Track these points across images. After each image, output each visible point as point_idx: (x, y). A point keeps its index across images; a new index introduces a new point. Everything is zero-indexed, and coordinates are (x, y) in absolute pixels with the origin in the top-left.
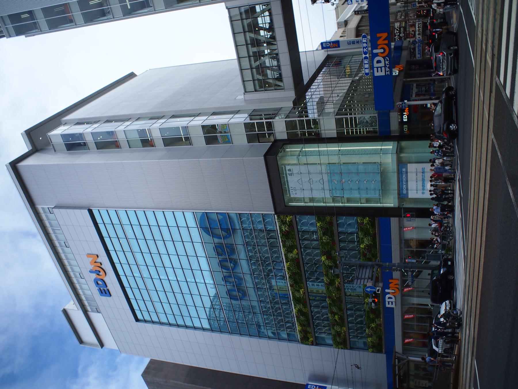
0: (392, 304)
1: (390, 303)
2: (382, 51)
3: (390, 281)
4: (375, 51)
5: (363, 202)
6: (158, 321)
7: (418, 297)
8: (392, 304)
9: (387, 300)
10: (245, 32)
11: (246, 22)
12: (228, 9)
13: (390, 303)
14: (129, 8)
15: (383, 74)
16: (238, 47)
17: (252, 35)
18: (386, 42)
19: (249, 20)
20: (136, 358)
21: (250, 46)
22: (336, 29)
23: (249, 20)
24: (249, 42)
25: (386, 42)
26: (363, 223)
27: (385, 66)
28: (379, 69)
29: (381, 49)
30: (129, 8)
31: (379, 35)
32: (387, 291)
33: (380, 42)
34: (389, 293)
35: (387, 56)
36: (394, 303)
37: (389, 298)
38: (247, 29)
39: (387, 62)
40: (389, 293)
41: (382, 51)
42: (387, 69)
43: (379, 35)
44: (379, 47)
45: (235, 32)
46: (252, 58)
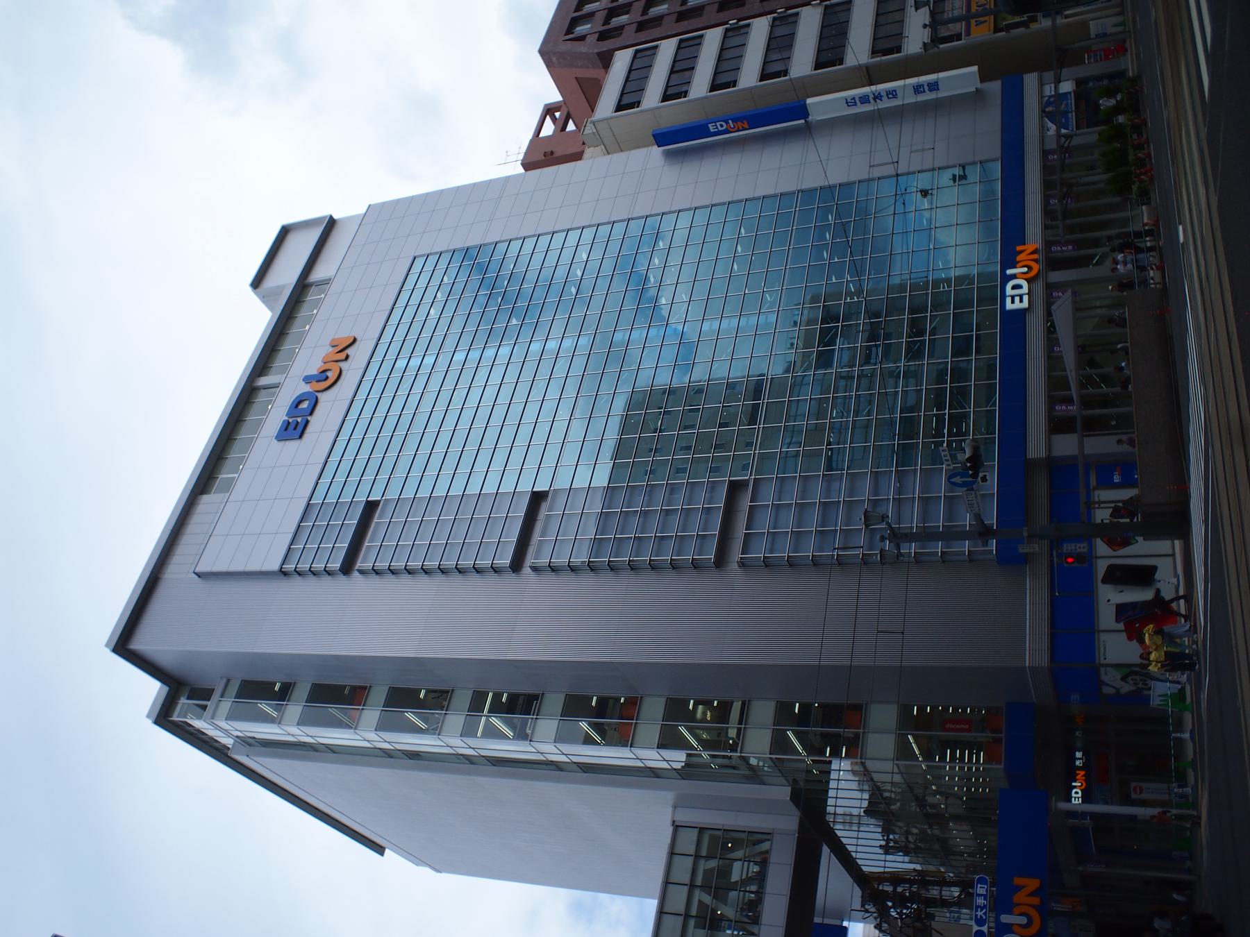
0: (1021, 301)
1: (1017, 299)
2: (1023, 920)
3: (1019, 248)
4: (1005, 919)
6: (548, 118)
8: (1021, 301)
9: (1009, 291)
10: (692, 886)
11: (703, 865)
12: (677, 827)
13: (1017, 299)
14: (504, 700)
16: (665, 916)
17: (707, 899)
19: (713, 864)
21: (692, 922)
23: (713, 864)
24: (694, 912)
29: (1021, 914)
30: (504, 700)
31: (1018, 881)
32: (1009, 272)
33: (1020, 897)
34: (1014, 277)
36: (1026, 298)
37: (1014, 287)
38: (699, 882)
40: (1014, 277)
41: (1023, 920)
43: (1018, 881)
45: (677, 851)
46: (692, 922)
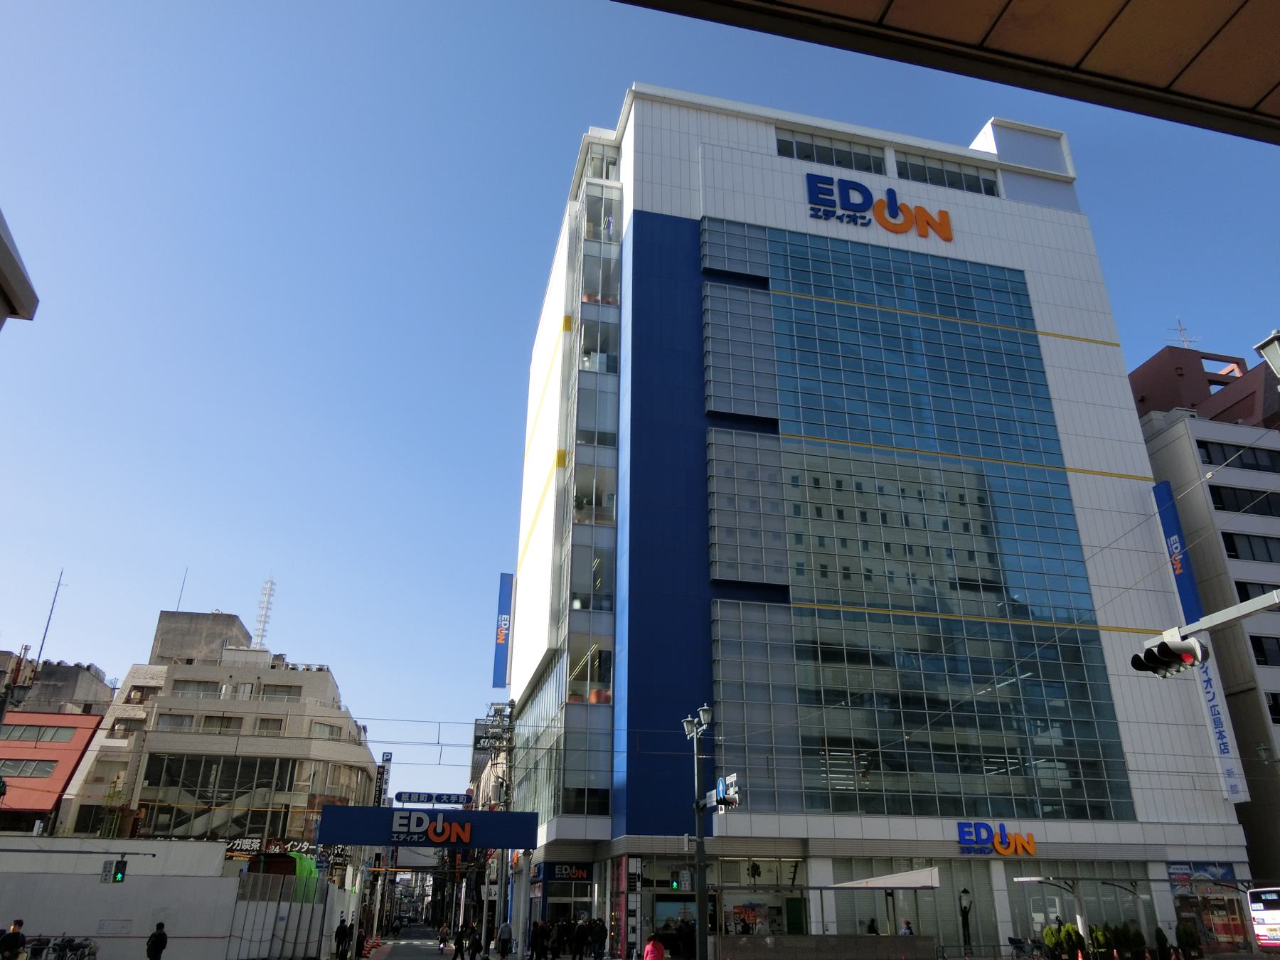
2: (439, 830)
5: (614, 254)
7: (715, 944)
15: (396, 828)
18: (453, 839)
20: (833, 930)
22: (145, 659)
25: (453, 839)
26: (1224, 925)
27: (409, 833)
28: (405, 822)
31: (468, 826)
35: (428, 837)
39: (416, 837)
41: (439, 830)
42: (402, 837)
44: (447, 824)
